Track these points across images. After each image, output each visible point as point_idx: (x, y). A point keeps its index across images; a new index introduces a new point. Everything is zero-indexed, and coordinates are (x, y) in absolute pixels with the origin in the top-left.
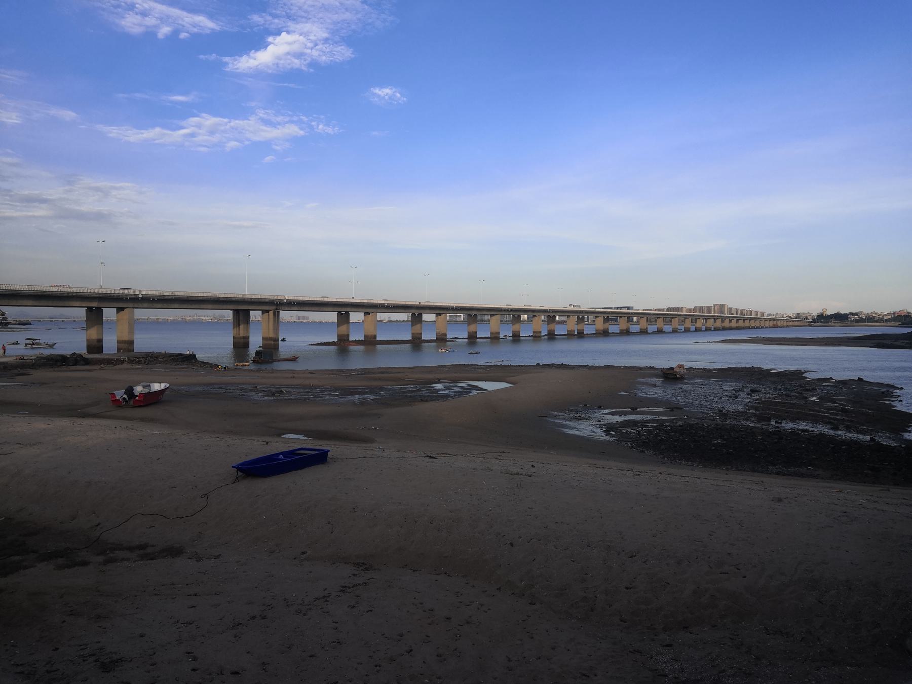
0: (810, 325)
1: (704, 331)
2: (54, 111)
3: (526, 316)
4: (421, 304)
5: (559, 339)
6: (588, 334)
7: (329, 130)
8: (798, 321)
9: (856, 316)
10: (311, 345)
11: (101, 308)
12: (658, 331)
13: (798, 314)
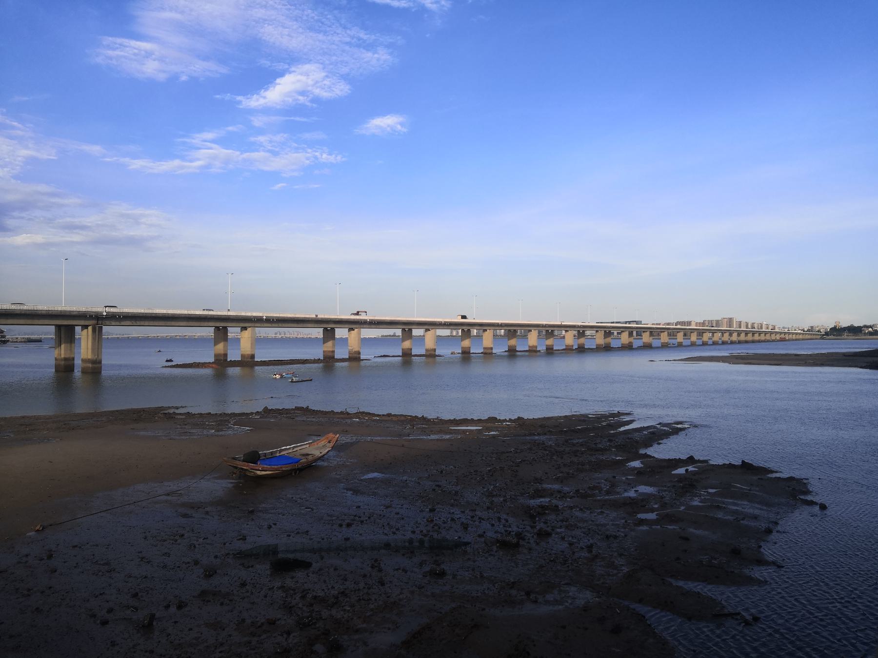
0: (822, 338)
1: (720, 344)
2: (86, 148)
3: (503, 331)
4: (319, 317)
5: (522, 356)
6: (559, 350)
7: (332, 159)
8: (809, 334)
9: (870, 329)
10: (381, 356)
11: (334, 328)
12: (644, 346)
13: (812, 327)
